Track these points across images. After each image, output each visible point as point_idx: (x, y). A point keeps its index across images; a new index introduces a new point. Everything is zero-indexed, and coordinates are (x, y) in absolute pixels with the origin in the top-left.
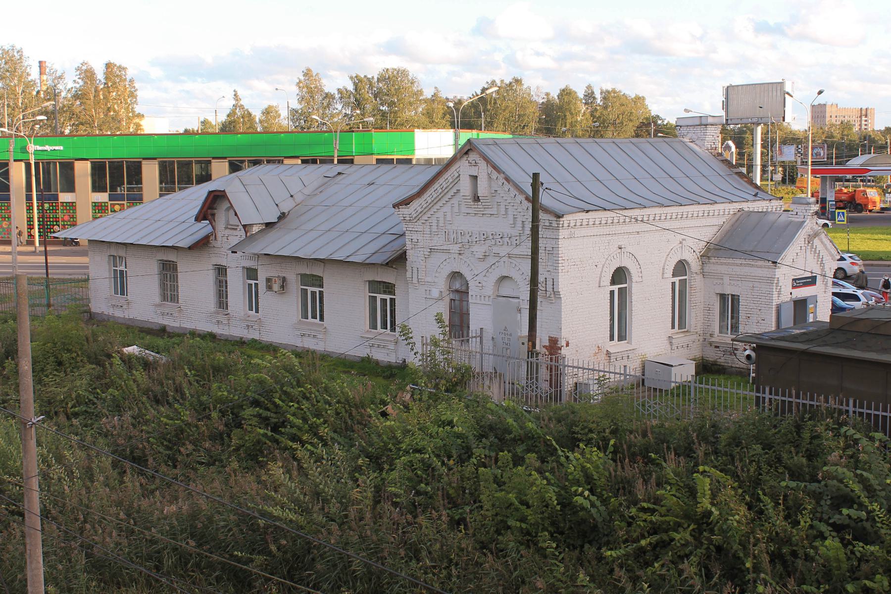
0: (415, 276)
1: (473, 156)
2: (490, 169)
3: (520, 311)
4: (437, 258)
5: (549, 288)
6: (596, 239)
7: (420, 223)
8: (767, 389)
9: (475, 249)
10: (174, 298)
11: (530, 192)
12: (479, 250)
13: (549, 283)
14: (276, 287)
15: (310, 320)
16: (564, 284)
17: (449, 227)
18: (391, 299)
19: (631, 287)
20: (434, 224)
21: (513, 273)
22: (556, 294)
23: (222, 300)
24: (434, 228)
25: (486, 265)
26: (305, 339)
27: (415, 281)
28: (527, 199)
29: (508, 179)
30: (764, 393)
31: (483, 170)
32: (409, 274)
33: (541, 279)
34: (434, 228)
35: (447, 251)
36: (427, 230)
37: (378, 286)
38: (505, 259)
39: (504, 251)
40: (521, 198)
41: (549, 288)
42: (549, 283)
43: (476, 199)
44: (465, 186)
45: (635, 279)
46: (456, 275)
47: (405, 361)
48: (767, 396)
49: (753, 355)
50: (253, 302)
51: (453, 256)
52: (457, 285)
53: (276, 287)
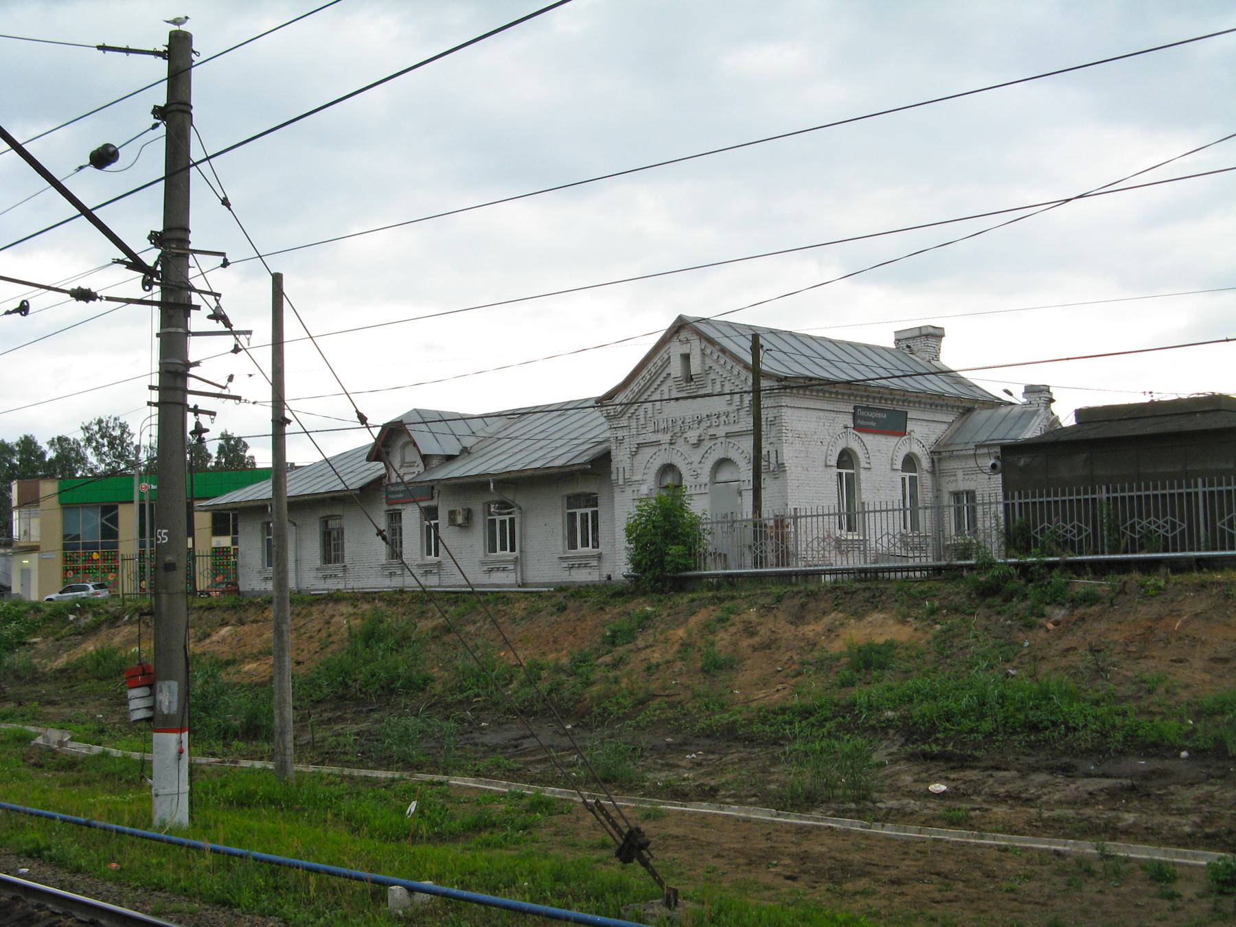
0: (621, 477)
1: (683, 335)
2: (704, 343)
3: (740, 494)
4: (646, 453)
5: (773, 460)
6: (821, 414)
7: (626, 417)
8: (1016, 494)
9: (689, 434)
10: (339, 559)
11: (749, 359)
12: (692, 435)
13: (773, 456)
14: (460, 520)
15: (499, 552)
16: (789, 455)
17: (658, 417)
18: (576, 548)
19: (859, 474)
20: (642, 416)
21: (733, 455)
22: (781, 467)
23: (395, 552)
24: (642, 421)
25: (701, 451)
26: (494, 574)
27: (621, 482)
28: (746, 367)
29: (724, 350)
30: (1013, 498)
31: (695, 347)
32: (614, 477)
33: (764, 452)
34: (642, 421)
35: (657, 443)
36: (634, 424)
37: (574, 501)
38: (723, 440)
39: (721, 431)
40: (738, 368)
41: (773, 460)
42: (773, 456)
43: (689, 378)
44: (676, 368)
45: (863, 464)
46: (668, 468)
47: (609, 578)
48: (1016, 501)
49: (999, 463)
50: (432, 541)
51: (663, 447)
52: (669, 480)
53: (460, 520)
